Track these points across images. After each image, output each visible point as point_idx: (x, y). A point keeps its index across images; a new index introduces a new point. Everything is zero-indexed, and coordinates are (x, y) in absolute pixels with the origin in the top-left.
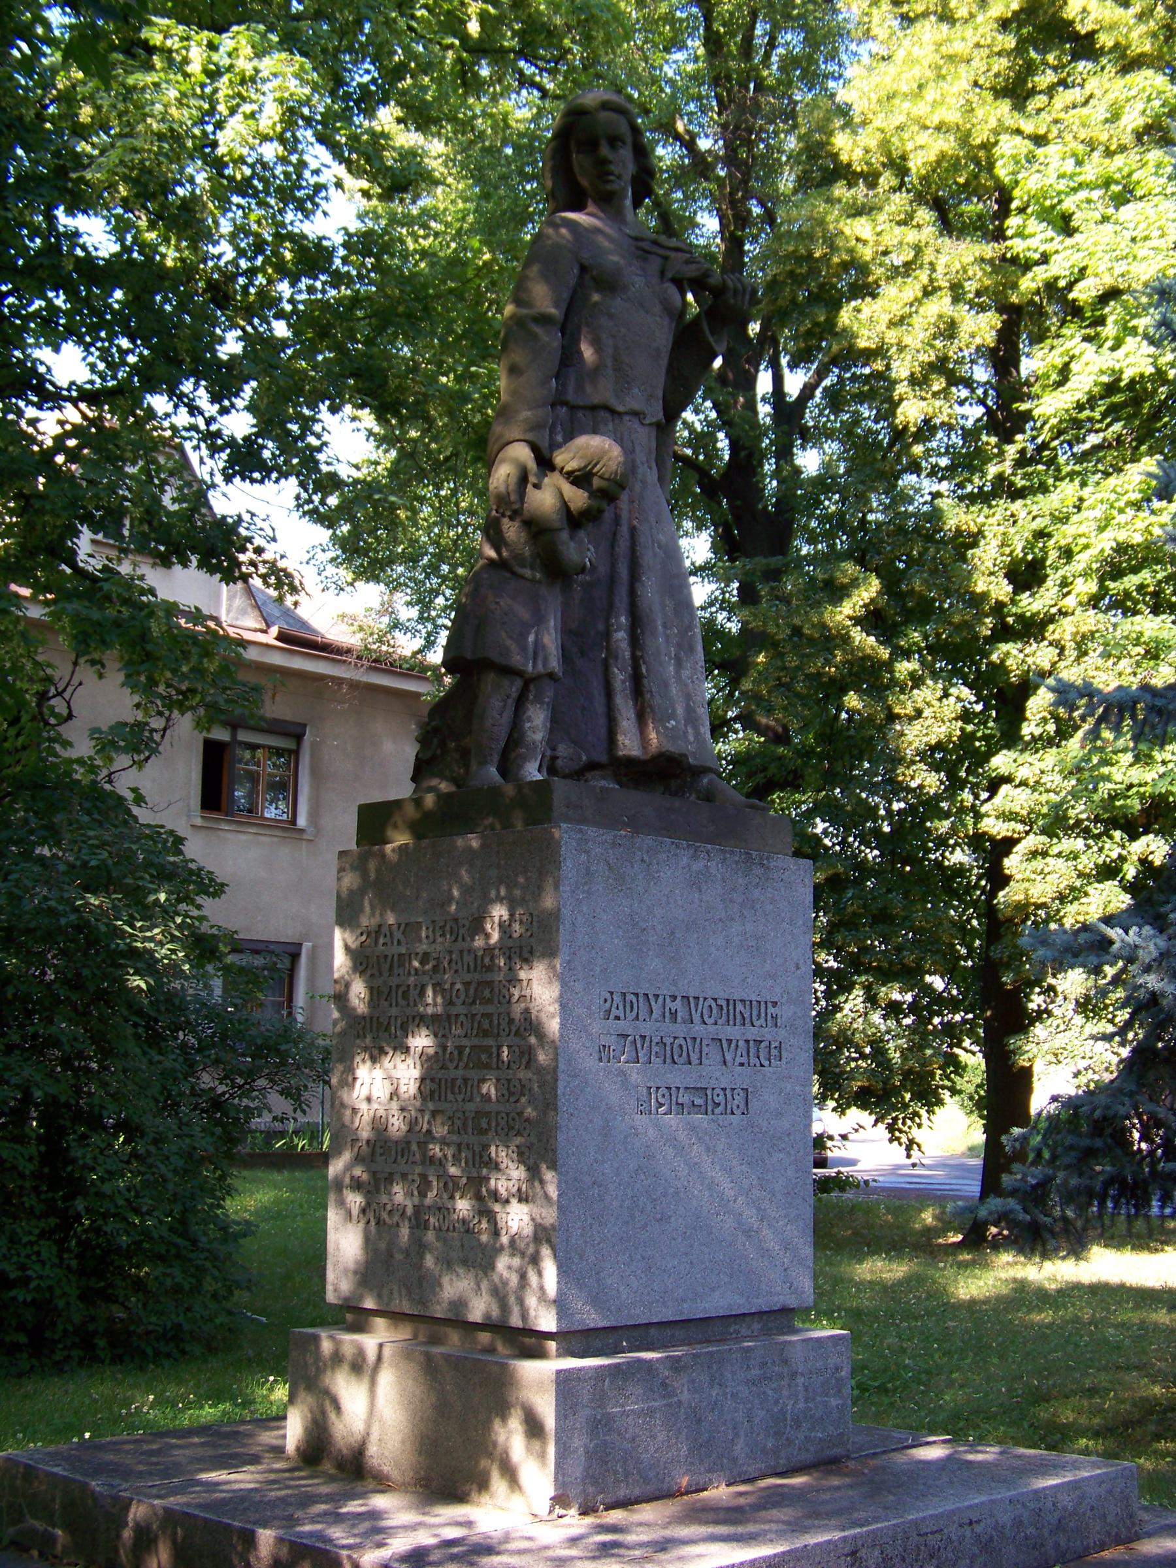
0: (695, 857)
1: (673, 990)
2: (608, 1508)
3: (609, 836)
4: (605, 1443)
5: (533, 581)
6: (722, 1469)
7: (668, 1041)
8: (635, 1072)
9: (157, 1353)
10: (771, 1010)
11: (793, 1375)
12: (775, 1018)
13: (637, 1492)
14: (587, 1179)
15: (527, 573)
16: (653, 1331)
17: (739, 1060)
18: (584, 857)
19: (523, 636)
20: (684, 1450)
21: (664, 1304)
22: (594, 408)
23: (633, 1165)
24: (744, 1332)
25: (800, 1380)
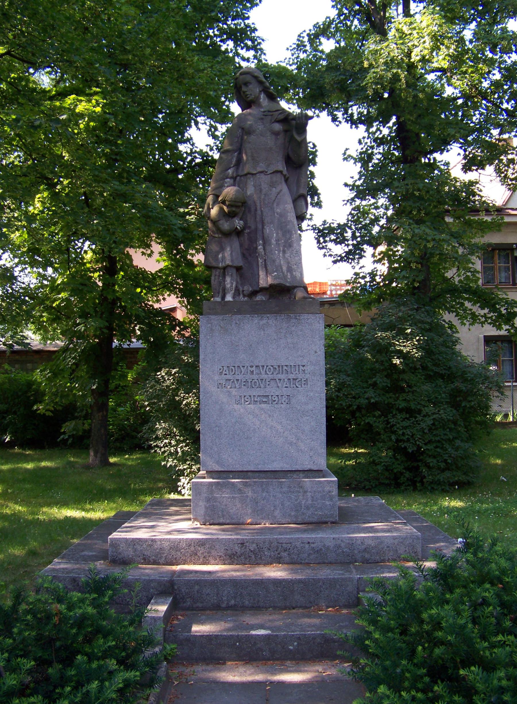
0: (262, 319)
1: (251, 364)
2: (210, 525)
3: (221, 317)
4: (213, 505)
5: (219, 238)
6: (269, 519)
7: (250, 381)
8: (234, 392)
9: (432, 488)
10: (301, 368)
11: (305, 492)
12: (304, 371)
13: (228, 521)
14: (214, 425)
15: (217, 235)
16: (249, 473)
17: (285, 386)
18: (209, 325)
19: (217, 256)
20: (250, 511)
21: (249, 465)
22: (246, 175)
23: (233, 420)
24: (295, 476)
25: (309, 494)
